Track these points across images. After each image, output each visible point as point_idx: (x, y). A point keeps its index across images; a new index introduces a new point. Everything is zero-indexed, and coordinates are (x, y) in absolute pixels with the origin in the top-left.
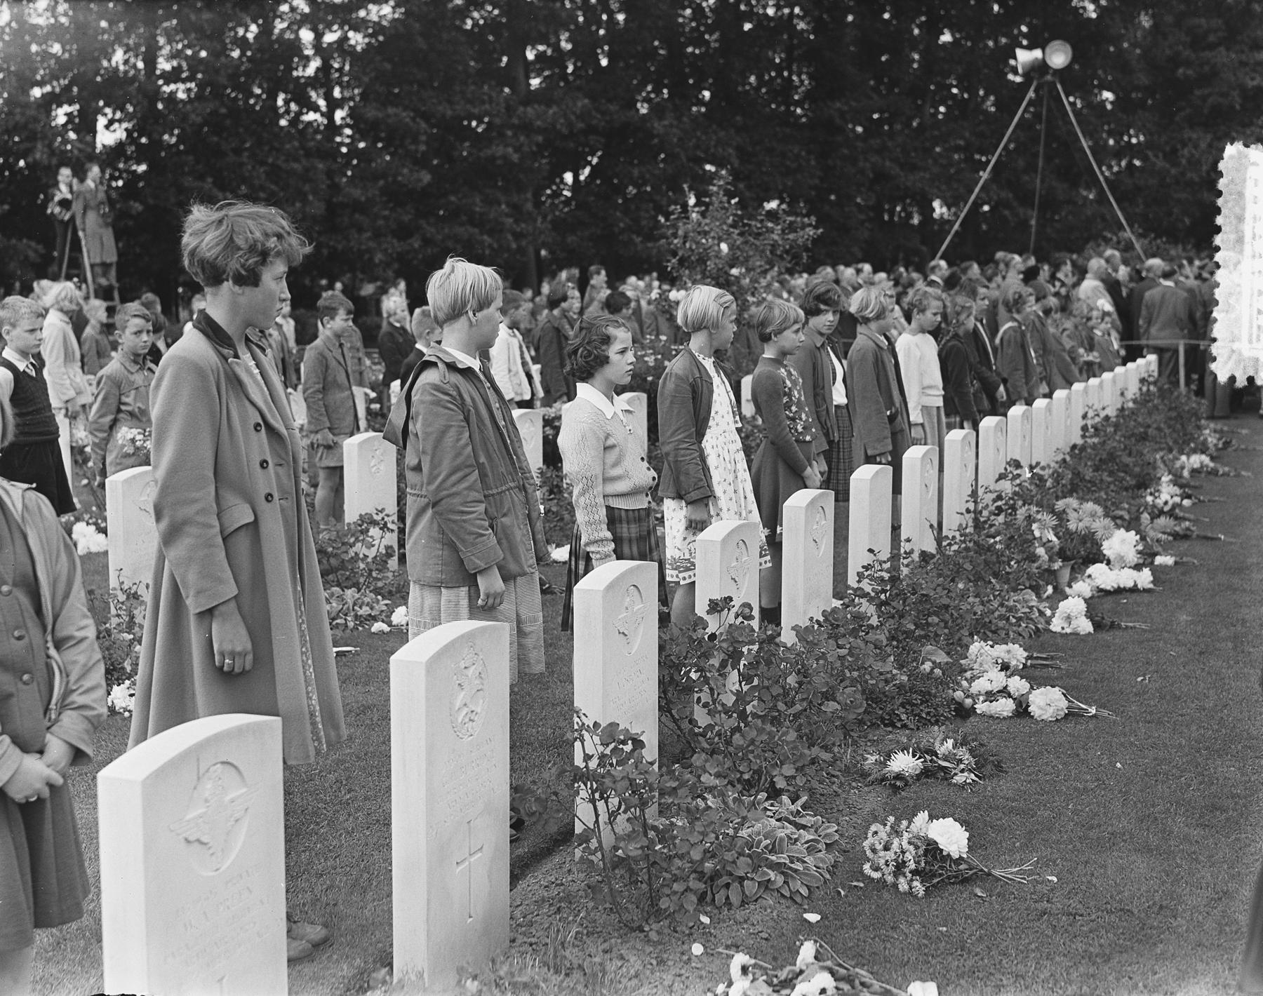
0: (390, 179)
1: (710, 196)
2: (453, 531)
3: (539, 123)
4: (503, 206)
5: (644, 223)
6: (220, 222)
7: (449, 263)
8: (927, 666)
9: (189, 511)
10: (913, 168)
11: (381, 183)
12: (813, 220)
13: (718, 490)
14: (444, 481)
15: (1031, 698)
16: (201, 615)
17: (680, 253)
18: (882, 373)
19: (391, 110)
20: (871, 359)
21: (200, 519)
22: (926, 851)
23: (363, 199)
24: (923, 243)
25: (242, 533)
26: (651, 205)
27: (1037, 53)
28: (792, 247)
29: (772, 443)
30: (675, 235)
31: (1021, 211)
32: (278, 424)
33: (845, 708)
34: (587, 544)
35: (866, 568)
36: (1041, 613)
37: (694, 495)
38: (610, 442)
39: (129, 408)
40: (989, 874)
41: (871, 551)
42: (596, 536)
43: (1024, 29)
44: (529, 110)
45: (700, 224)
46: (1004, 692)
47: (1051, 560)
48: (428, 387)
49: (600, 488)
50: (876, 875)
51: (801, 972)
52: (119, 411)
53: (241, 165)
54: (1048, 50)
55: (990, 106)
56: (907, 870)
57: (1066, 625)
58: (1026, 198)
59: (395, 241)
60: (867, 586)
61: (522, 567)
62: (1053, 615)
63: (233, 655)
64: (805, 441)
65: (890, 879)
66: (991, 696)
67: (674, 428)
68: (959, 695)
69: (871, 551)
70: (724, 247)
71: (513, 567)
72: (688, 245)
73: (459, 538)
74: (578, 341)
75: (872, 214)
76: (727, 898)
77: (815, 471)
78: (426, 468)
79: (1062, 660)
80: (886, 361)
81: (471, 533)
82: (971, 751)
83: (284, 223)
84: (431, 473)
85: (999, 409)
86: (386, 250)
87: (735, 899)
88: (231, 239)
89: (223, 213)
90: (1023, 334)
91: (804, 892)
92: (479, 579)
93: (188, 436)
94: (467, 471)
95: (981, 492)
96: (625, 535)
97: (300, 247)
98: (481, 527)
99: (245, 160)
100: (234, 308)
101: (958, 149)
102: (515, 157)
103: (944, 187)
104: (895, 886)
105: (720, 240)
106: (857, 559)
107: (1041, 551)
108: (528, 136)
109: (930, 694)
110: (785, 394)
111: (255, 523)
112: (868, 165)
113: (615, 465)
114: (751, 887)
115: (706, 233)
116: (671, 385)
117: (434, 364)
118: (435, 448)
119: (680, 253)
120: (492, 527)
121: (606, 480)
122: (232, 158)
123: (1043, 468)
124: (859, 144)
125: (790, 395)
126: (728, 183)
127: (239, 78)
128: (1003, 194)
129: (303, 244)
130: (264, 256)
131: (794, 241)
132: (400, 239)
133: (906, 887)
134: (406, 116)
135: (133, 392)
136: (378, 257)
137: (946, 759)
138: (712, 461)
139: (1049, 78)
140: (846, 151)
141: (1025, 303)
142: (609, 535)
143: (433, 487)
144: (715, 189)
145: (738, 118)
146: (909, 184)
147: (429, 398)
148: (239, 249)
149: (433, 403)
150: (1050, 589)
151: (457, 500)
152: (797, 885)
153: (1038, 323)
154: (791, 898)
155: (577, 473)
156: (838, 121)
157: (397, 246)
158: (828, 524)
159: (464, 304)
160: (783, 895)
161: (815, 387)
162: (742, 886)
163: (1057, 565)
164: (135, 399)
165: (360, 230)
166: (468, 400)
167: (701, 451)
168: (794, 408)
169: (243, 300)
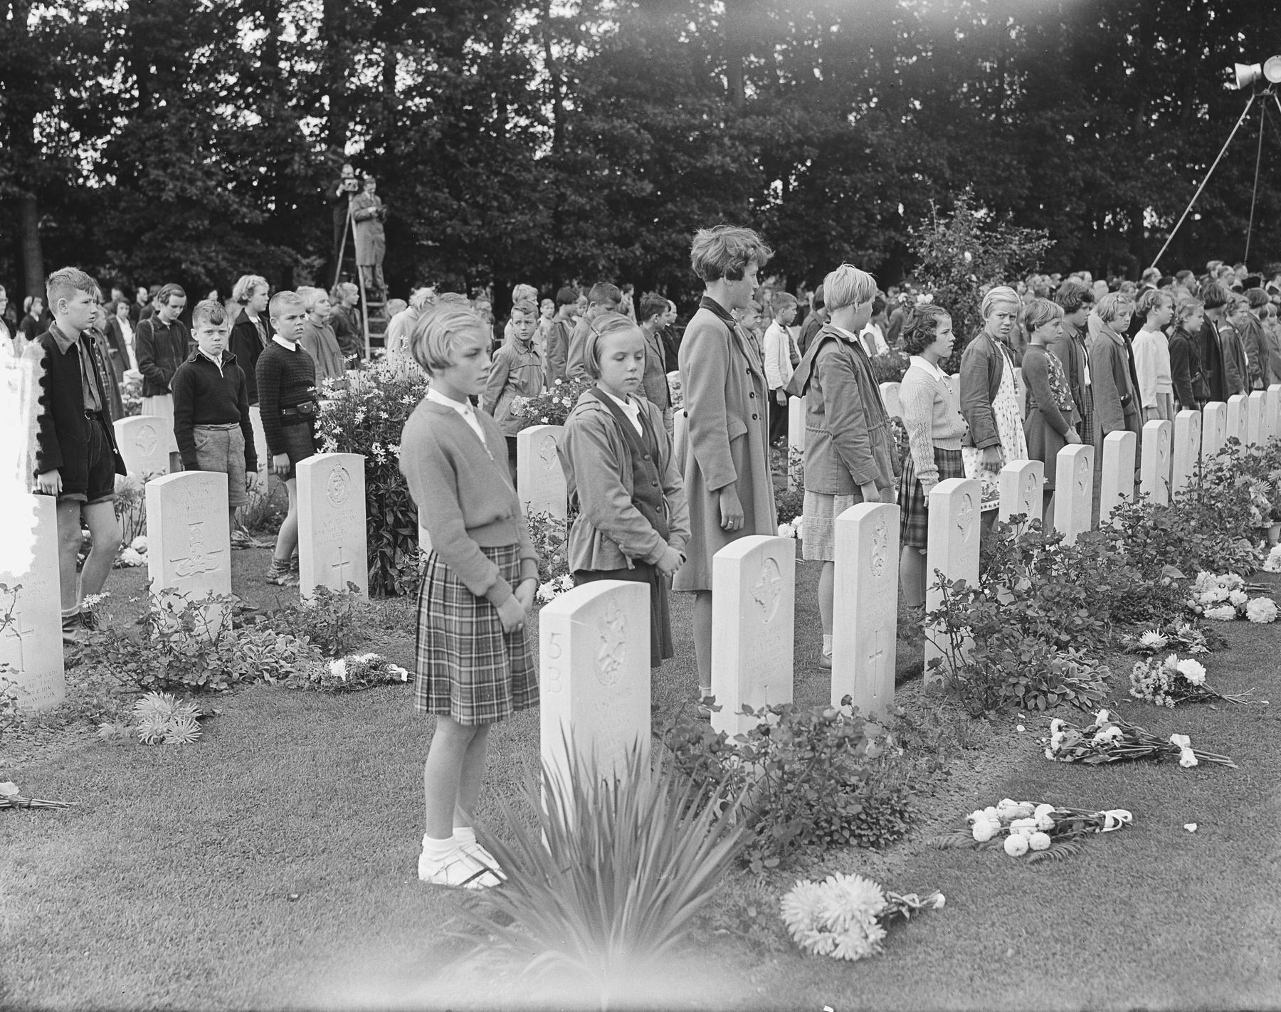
0: (614, 188)
1: (954, 210)
2: (847, 455)
3: (757, 134)
4: (721, 214)
5: (855, 231)
6: (717, 239)
7: (842, 269)
8: (1167, 581)
9: (714, 423)
10: (1124, 177)
11: (606, 192)
12: (1047, 232)
13: (1004, 442)
14: (842, 421)
15: (1249, 605)
16: (712, 493)
17: (926, 261)
18: (1118, 366)
19: (617, 122)
20: (1108, 353)
21: (718, 429)
22: (1176, 680)
23: (588, 207)
24: (1132, 251)
25: (740, 439)
26: (863, 213)
27: (1256, 68)
28: (1027, 256)
29: (1041, 411)
30: (921, 245)
31: (1235, 220)
32: (759, 371)
33: (1115, 588)
34: (919, 474)
35: (1117, 508)
36: (1255, 557)
37: (987, 443)
38: (939, 398)
39: (515, 382)
40: (1220, 698)
41: (1121, 495)
42: (927, 467)
43: (1241, 36)
44: (748, 120)
45: (944, 235)
46: (1227, 601)
47: (1264, 519)
48: (831, 356)
49: (930, 432)
50: (1139, 696)
51: (1099, 728)
52: (507, 383)
53: (477, 175)
54: (1266, 64)
55: (1203, 112)
56: (1162, 692)
57: (1276, 566)
58: (1241, 208)
59: (617, 247)
60: (1118, 524)
61: (888, 481)
62: (1266, 559)
63: (735, 518)
64: (1066, 410)
65: (1149, 697)
66: (1216, 604)
67: (972, 392)
68: (1191, 603)
69: (1121, 495)
70: (968, 255)
71: (884, 482)
72: (934, 254)
73: (850, 459)
74: (912, 325)
75: (1081, 223)
76: (1036, 705)
77: (1072, 433)
78: (828, 410)
79: (1273, 587)
80: (1122, 355)
81: (860, 457)
82: (1203, 633)
83: (757, 239)
84: (832, 416)
85: (1221, 396)
86: (609, 256)
87: (1041, 705)
88: (726, 250)
89: (717, 233)
90: (1237, 337)
91: (1090, 704)
92: (863, 490)
93: (713, 376)
94: (858, 414)
95: (1204, 459)
96: (946, 469)
97: (766, 254)
98: (867, 453)
99: (481, 171)
100: (726, 295)
101: (1170, 158)
102: (733, 167)
103: (1155, 197)
104: (1153, 702)
105: (963, 250)
106: (1109, 501)
107: (1254, 510)
108: (746, 146)
109: (1168, 600)
110: (1050, 372)
111: (746, 436)
112: (1078, 173)
113: (941, 416)
114: (1052, 698)
115: (950, 243)
116: (972, 359)
117: (833, 340)
118: (836, 398)
119: (926, 261)
120: (872, 453)
121: (934, 427)
122: (468, 168)
123: (1258, 449)
124: (1071, 153)
125: (1053, 373)
126: (971, 198)
127: (477, 93)
128: (1216, 204)
129: (768, 253)
130: (746, 259)
131: (1030, 250)
132: (621, 247)
133: (1162, 702)
134: (630, 127)
135: (520, 369)
136: (602, 264)
137: (1184, 636)
138: (999, 418)
139: (1267, 91)
140: (1056, 160)
141: (1237, 308)
142: (936, 467)
143: (833, 426)
144: (960, 203)
145: (950, 127)
146: (1120, 193)
147: (832, 363)
148: (731, 256)
149: (835, 366)
150: (1263, 544)
151: (852, 434)
152: (1083, 698)
153: (1255, 326)
154: (1080, 708)
155: (915, 421)
156: (1050, 131)
157: (620, 253)
158: (1089, 472)
159: (853, 297)
160: (1074, 705)
161: (1071, 370)
162: (1047, 699)
163: (1269, 524)
164: (521, 375)
165: (585, 237)
166: (857, 365)
167: (993, 410)
168: (1057, 383)
169: (731, 289)
